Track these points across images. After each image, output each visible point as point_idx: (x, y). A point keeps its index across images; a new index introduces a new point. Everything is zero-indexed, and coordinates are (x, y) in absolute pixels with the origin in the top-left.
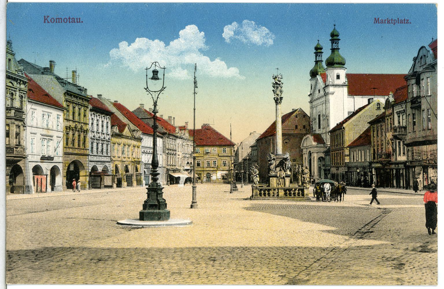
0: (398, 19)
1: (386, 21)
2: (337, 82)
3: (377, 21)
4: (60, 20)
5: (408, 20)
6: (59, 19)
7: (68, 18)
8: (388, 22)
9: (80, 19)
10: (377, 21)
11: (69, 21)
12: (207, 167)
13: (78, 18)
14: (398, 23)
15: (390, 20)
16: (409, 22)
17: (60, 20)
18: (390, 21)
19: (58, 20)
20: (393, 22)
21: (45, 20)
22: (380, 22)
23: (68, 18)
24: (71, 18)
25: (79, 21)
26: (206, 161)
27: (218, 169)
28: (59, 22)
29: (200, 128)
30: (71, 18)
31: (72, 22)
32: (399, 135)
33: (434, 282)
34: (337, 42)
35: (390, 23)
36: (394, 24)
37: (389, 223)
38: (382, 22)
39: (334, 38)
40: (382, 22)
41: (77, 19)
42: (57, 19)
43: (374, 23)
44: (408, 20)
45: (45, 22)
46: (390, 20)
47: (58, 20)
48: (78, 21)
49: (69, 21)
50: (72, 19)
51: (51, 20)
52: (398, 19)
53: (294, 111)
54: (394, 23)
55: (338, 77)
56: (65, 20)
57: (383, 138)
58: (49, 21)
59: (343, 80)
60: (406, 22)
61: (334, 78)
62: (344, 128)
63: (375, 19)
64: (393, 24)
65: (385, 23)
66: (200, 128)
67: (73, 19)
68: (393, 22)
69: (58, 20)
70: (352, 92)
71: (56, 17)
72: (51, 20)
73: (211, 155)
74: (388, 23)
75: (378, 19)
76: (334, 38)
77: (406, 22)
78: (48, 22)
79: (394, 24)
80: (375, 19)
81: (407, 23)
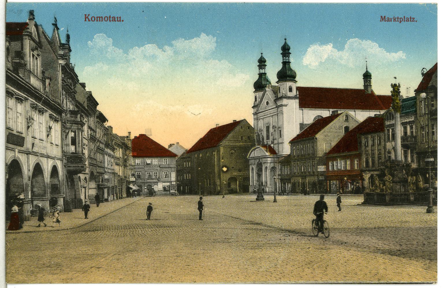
0: (404, 17)
1: (393, 20)
2: (289, 94)
3: (383, 19)
4: (101, 18)
5: (414, 18)
6: (100, 17)
7: (108, 16)
8: (395, 20)
9: (120, 18)
10: (383, 19)
11: (110, 19)
12: (148, 179)
13: (119, 16)
14: (404, 21)
15: (396, 18)
16: (415, 20)
17: (101, 18)
18: (397, 19)
19: (99, 19)
20: (399, 20)
21: (86, 18)
22: (386, 19)
23: (108, 16)
24: (112, 16)
25: (119, 19)
26: (147, 172)
27: (159, 181)
28: (100, 21)
29: (392, 88)
30: (112, 16)
31: (112, 21)
32: (410, 144)
33: (433, 7)
34: (288, 56)
35: (396, 21)
36: (400, 22)
37: (215, 258)
38: (389, 20)
39: (286, 51)
40: (407, 20)
41: (118, 18)
42: (97, 17)
43: (381, 21)
44: (414, 18)
45: (86, 20)
46: (396, 18)
47: (99, 19)
48: (119, 20)
49: (110, 19)
50: (113, 18)
51: (92, 19)
52: (404, 17)
53: (235, 124)
54: (400, 21)
55: (291, 90)
56: (106, 19)
57: (382, 147)
58: (90, 19)
59: (294, 92)
60: (412, 20)
61: (287, 90)
62: (316, 138)
63: (382, 17)
64: (399, 22)
65: (391, 21)
66: (392, 88)
67: (114, 18)
68: (399, 20)
69: (98, 18)
70: (303, 105)
71: (96, 16)
72: (92, 19)
73: (152, 166)
74: (394, 21)
75: (385, 17)
76: (286, 51)
77: (412, 20)
78: (89, 20)
79: (400, 22)
80: (382, 17)
81: (412, 21)
